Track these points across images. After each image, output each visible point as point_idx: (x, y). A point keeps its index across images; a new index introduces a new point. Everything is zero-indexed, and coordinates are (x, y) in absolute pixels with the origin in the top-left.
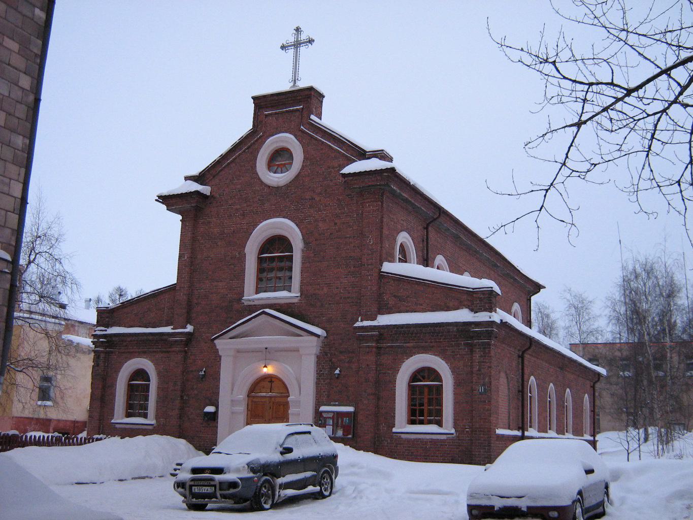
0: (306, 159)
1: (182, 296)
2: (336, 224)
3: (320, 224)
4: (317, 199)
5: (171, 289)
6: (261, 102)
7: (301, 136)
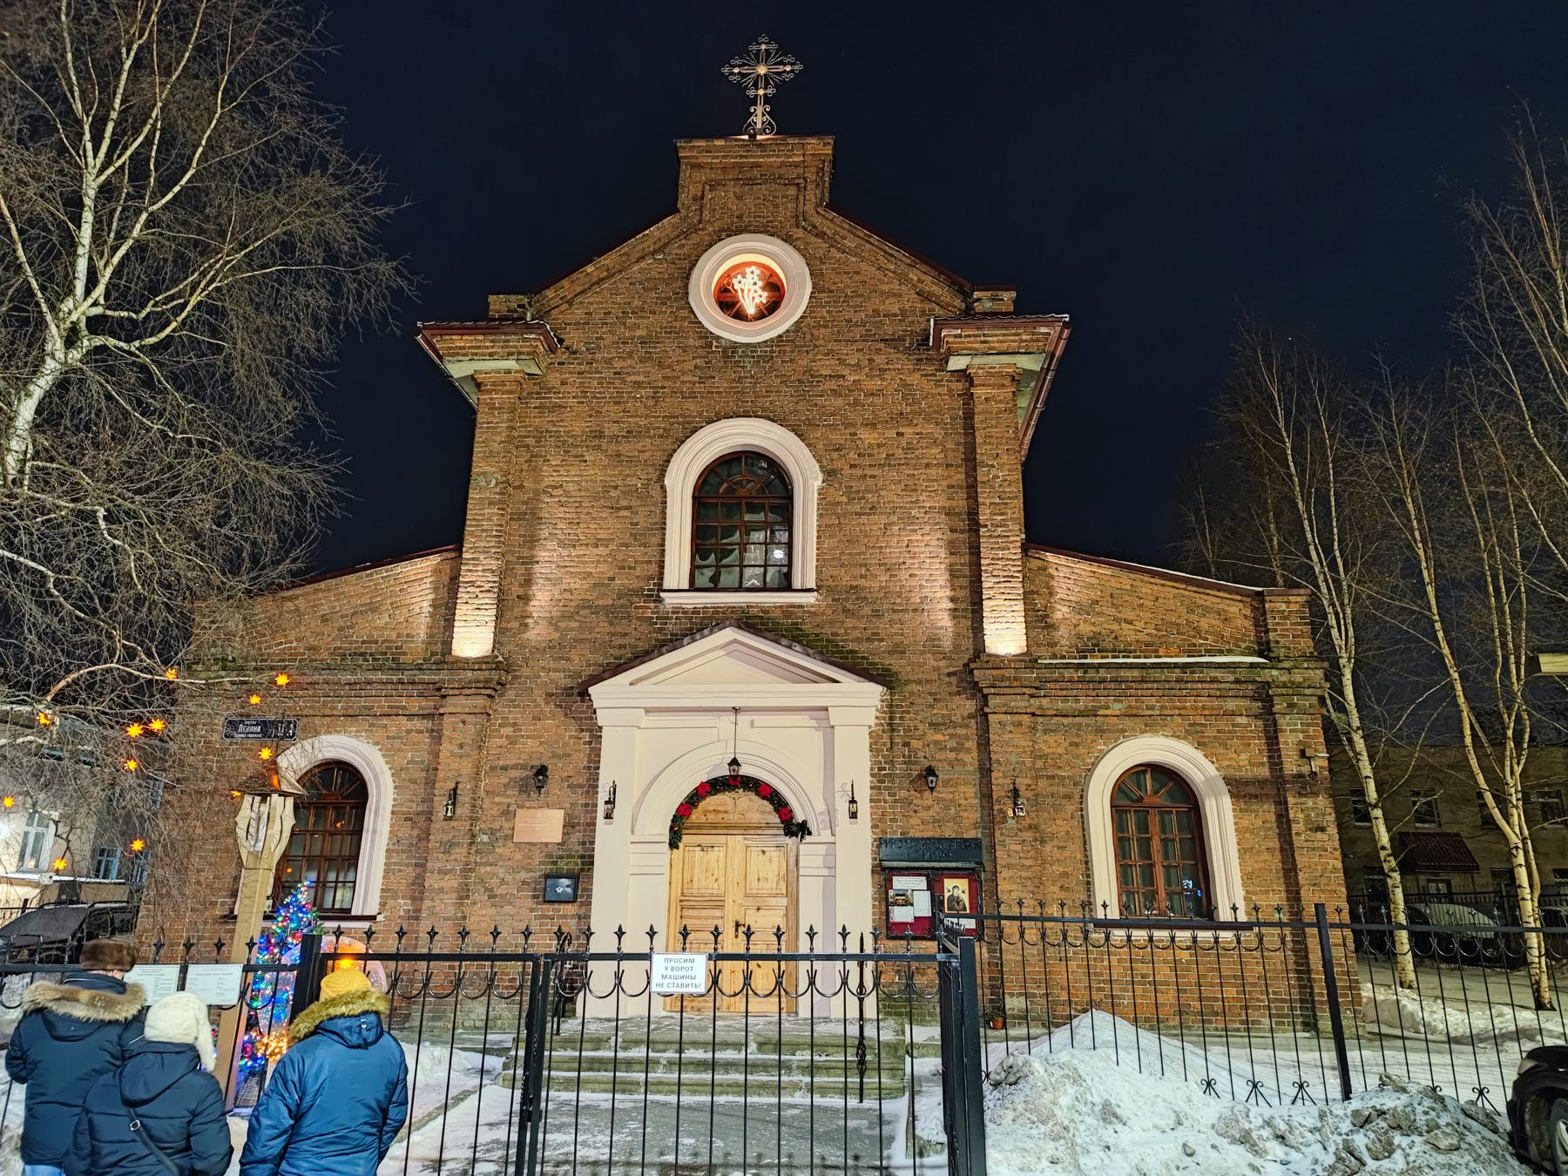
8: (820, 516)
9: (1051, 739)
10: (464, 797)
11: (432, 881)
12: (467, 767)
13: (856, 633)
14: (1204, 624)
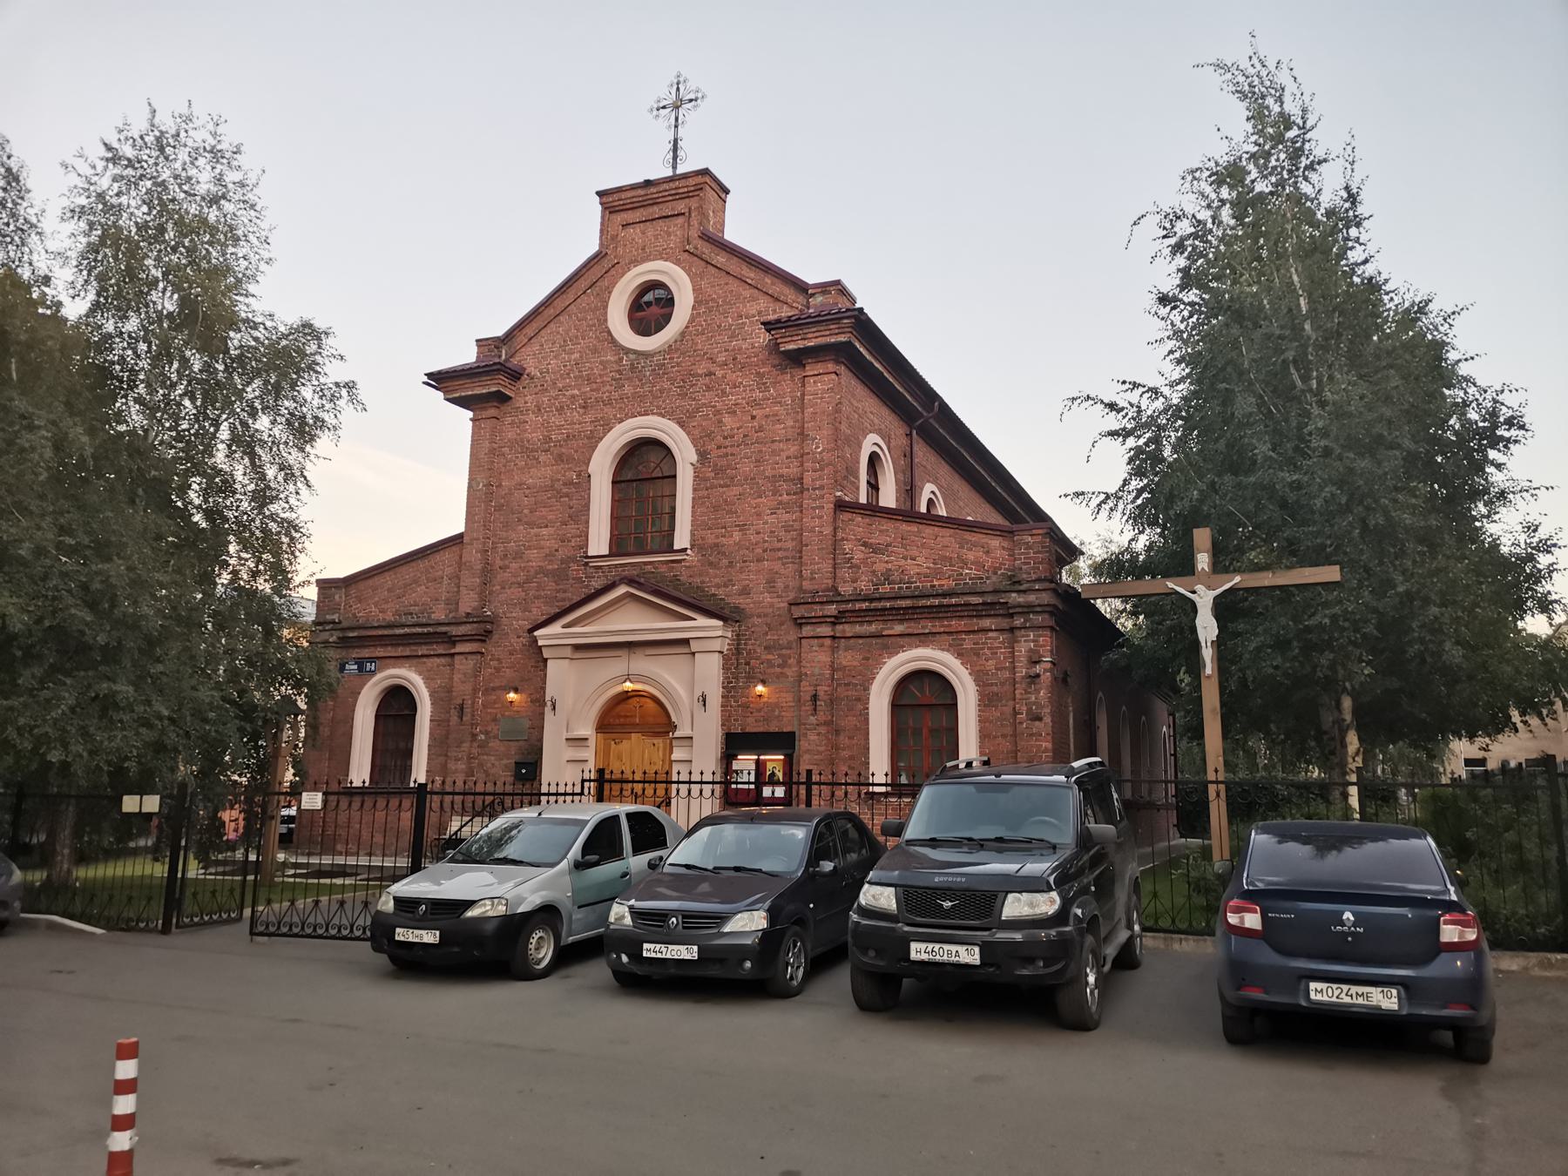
0: (698, 303)
1: (472, 555)
2: (753, 417)
3: (727, 419)
4: (719, 373)
5: (457, 540)
6: (614, 202)
7: (687, 256)
8: (695, 490)
9: (849, 655)
10: (467, 710)
11: (452, 766)
12: (468, 687)
13: (717, 580)
14: (971, 556)
